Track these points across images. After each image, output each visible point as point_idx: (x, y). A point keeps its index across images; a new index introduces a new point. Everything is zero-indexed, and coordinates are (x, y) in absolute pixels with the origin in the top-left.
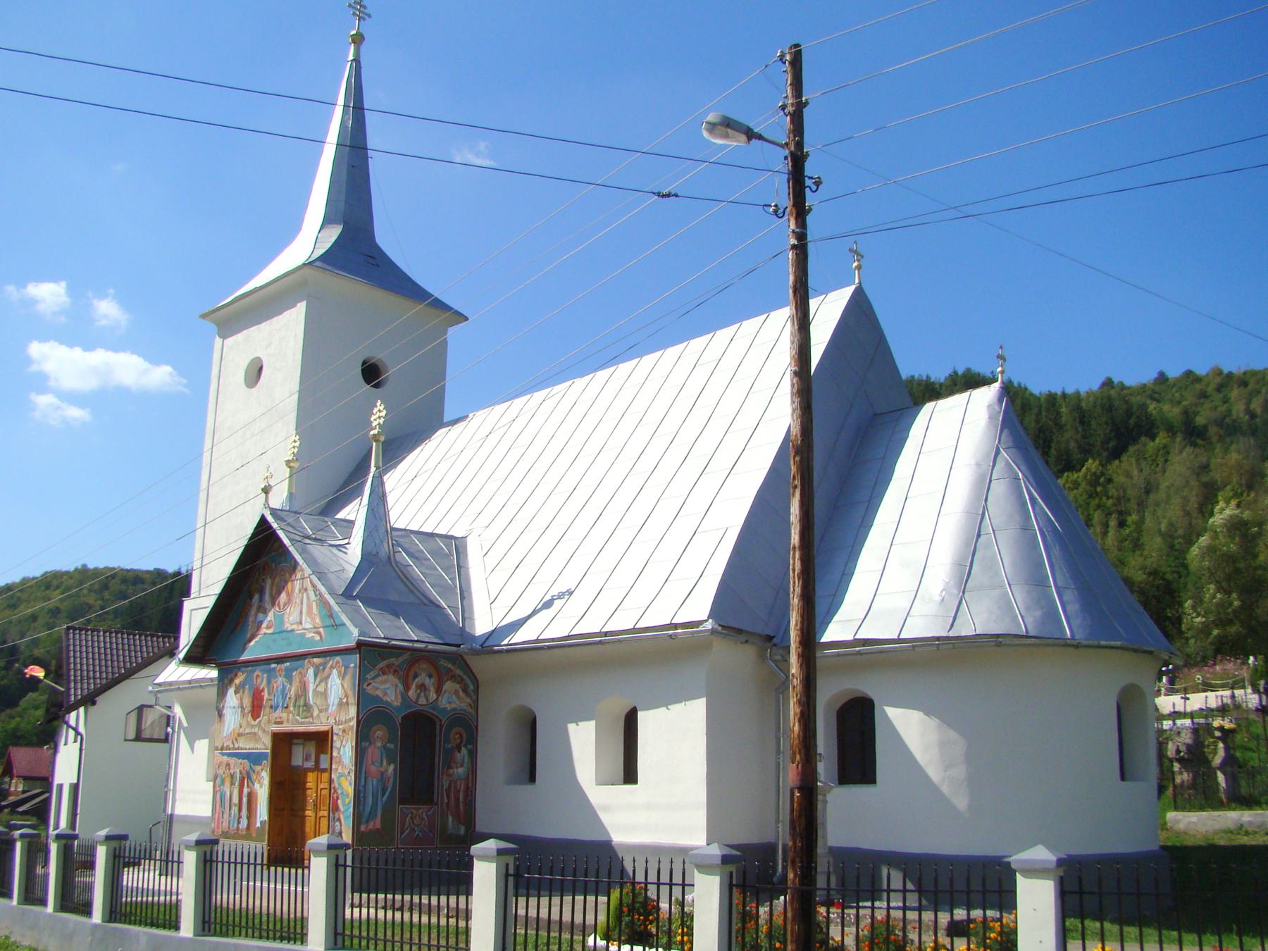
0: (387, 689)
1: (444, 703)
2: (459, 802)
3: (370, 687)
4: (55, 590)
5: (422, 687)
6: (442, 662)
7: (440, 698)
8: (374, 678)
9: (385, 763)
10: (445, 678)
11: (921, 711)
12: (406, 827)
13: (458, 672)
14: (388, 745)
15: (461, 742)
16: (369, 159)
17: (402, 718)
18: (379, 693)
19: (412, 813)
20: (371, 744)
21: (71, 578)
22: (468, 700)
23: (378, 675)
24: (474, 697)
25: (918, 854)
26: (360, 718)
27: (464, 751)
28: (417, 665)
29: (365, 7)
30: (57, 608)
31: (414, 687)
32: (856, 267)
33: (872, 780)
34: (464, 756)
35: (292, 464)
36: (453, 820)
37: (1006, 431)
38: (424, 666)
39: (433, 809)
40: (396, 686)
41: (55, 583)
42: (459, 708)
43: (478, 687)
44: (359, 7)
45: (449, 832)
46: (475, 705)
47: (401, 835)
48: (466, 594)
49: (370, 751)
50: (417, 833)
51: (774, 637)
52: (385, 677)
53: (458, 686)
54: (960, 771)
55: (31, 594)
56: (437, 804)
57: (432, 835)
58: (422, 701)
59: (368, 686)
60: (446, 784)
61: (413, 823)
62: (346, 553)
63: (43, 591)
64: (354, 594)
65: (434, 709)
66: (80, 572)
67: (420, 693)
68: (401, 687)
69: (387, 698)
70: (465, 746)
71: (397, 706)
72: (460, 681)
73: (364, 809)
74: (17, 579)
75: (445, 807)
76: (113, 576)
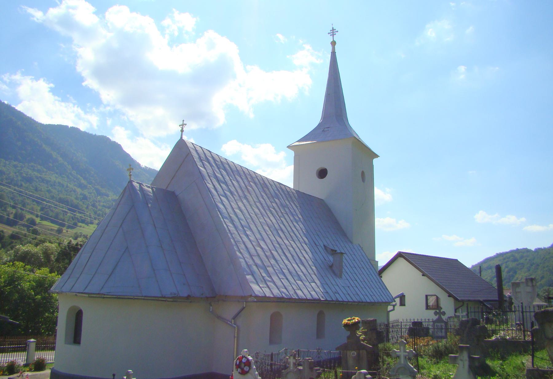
33: (400, 306)
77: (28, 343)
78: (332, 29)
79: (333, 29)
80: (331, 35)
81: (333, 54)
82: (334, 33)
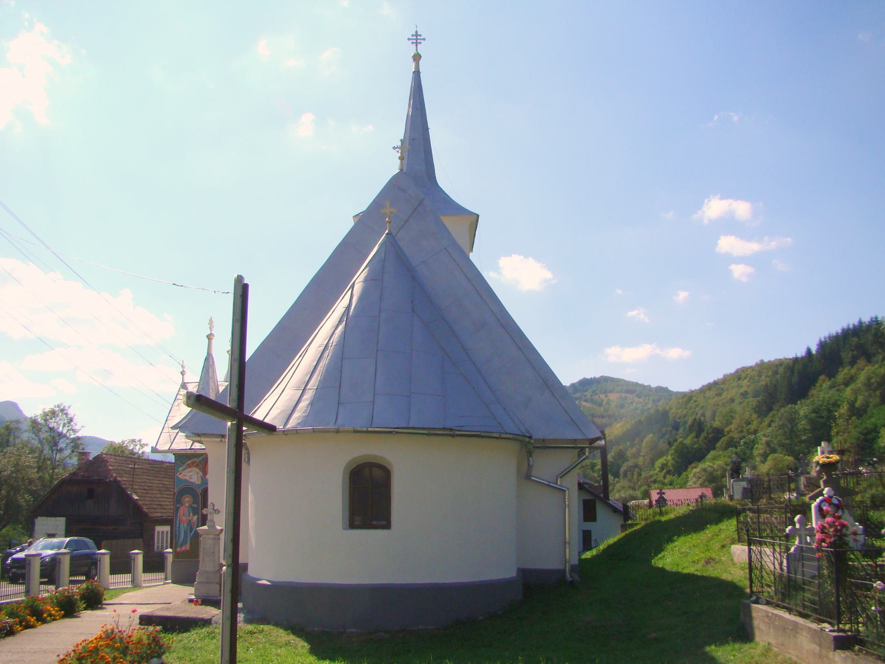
0: (192, 475)
3: (181, 475)
4: (743, 380)
8: (184, 470)
9: (191, 515)
14: (193, 505)
17: (202, 490)
18: (187, 478)
20: (182, 505)
21: (753, 370)
23: (186, 468)
30: (746, 392)
33: (388, 526)
40: (198, 473)
41: (743, 375)
49: (182, 509)
52: (190, 469)
55: (729, 385)
59: (180, 474)
63: (737, 382)
66: (758, 366)
68: (201, 474)
69: (192, 480)
71: (199, 484)
73: (179, 540)
74: (721, 376)
76: (781, 365)
77: (133, 556)
78: (414, 34)
79: (417, 35)
80: (413, 43)
81: (417, 74)
82: (418, 41)
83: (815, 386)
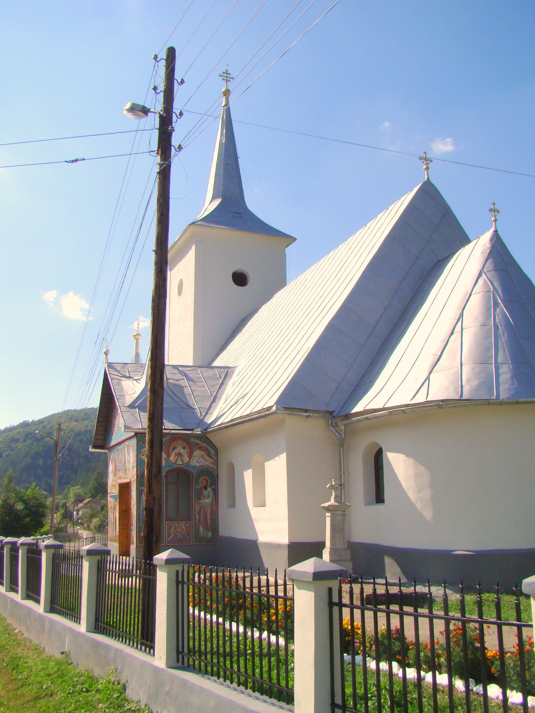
1: (194, 462)
2: (207, 519)
5: (179, 454)
6: (192, 440)
7: (191, 460)
10: (195, 448)
11: (404, 454)
12: (171, 533)
13: (203, 444)
15: (207, 484)
16: (239, 158)
19: (175, 526)
22: (212, 460)
24: (215, 459)
25: (404, 549)
26: (138, 474)
27: (209, 489)
28: (175, 442)
29: (230, 74)
31: (173, 455)
32: (425, 168)
34: (209, 494)
35: (136, 337)
36: (203, 530)
37: (490, 260)
38: (180, 442)
39: (188, 524)
42: (205, 465)
43: (217, 452)
44: (226, 75)
45: (201, 536)
46: (216, 462)
47: (168, 538)
48: (217, 400)
50: (179, 536)
51: (333, 412)
53: (203, 453)
54: (427, 494)
56: (192, 520)
57: (189, 538)
58: (180, 462)
59: (142, 456)
60: (197, 510)
61: (176, 532)
62: (139, 383)
64: (136, 406)
65: (186, 466)
67: (177, 458)
70: (210, 486)
72: (205, 450)
75: (197, 522)
78: (225, 71)
79: (226, 72)
83: (517, 645)
